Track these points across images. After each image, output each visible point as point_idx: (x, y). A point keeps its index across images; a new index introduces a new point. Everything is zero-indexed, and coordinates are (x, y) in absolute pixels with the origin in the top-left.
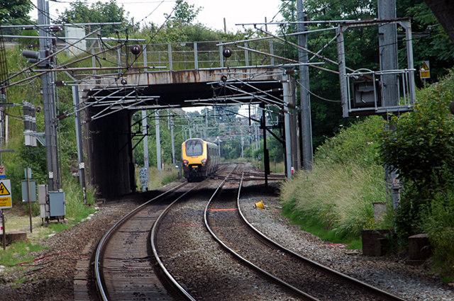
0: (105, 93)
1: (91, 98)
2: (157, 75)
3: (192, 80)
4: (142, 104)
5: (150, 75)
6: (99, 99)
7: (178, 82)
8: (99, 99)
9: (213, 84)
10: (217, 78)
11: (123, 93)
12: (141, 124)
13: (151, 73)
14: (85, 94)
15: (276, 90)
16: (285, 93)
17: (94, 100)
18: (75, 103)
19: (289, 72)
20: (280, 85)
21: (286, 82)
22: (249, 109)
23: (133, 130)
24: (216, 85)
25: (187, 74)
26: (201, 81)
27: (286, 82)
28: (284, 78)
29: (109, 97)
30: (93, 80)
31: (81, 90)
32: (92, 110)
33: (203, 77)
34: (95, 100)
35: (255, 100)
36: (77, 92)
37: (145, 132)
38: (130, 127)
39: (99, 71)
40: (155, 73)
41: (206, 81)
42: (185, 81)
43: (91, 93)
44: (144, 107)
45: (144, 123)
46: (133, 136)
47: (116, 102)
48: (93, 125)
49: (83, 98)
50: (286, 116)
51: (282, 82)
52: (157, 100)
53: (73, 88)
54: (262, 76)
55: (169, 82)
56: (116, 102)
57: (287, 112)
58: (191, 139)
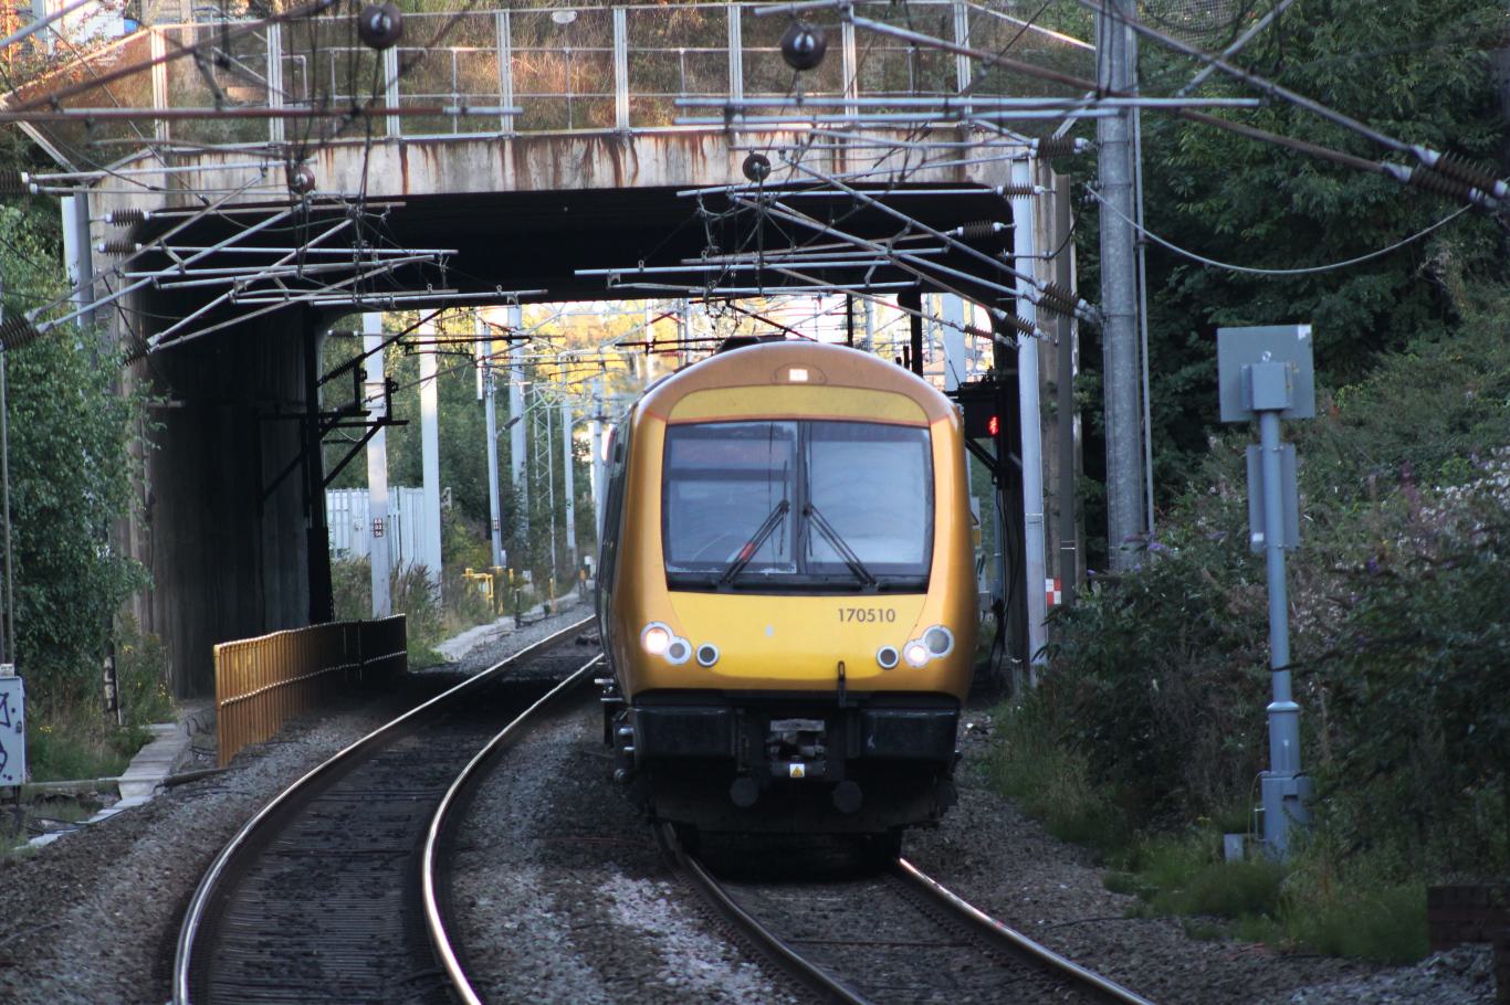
0: (212, 228)
1: (150, 254)
2: (442, 150)
3: (602, 176)
4: (381, 284)
5: (412, 151)
6: (184, 255)
7: (626, 183)
8: (184, 255)
9: (705, 196)
10: (716, 171)
11: (286, 233)
12: (360, 376)
13: (422, 144)
14: (121, 233)
15: (979, 228)
16: (1024, 242)
17: (161, 261)
18: (72, 271)
19: (1053, 155)
20: (998, 206)
21: (1026, 191)
22: (850, 314)
23: (331, 397)
24: (718, 200)
25: (578, 148)
26: (641, 182)
27: (1026, 191)
28: (1020, 176)
29: (222, 247)
30: (198, 129)
31: (102, 212)
32: (157, 306)
33: (648, 166)
34: (170, 262)
35: (884, 274)
36: (85, 223)
37: (376, 411)
38: (313, 385)
39: (183, 124)
40: (434, 144)
41: (673, 182)
42: (571, 181)
43: (146, 229)
44: (388, 297)
45: (374, 369)
46: (327, 428)
47: (263, 272)
48: (167, 370)
49: (109, 249)
50: (1026, 346)
51: (1011, 191)
52: (442, 266)
53: (67, 204)
54: (927, 167)
55: (499, 188)
56: (263, 272)
57: (1029, 331)
58: (1322, 701)
